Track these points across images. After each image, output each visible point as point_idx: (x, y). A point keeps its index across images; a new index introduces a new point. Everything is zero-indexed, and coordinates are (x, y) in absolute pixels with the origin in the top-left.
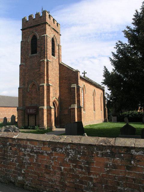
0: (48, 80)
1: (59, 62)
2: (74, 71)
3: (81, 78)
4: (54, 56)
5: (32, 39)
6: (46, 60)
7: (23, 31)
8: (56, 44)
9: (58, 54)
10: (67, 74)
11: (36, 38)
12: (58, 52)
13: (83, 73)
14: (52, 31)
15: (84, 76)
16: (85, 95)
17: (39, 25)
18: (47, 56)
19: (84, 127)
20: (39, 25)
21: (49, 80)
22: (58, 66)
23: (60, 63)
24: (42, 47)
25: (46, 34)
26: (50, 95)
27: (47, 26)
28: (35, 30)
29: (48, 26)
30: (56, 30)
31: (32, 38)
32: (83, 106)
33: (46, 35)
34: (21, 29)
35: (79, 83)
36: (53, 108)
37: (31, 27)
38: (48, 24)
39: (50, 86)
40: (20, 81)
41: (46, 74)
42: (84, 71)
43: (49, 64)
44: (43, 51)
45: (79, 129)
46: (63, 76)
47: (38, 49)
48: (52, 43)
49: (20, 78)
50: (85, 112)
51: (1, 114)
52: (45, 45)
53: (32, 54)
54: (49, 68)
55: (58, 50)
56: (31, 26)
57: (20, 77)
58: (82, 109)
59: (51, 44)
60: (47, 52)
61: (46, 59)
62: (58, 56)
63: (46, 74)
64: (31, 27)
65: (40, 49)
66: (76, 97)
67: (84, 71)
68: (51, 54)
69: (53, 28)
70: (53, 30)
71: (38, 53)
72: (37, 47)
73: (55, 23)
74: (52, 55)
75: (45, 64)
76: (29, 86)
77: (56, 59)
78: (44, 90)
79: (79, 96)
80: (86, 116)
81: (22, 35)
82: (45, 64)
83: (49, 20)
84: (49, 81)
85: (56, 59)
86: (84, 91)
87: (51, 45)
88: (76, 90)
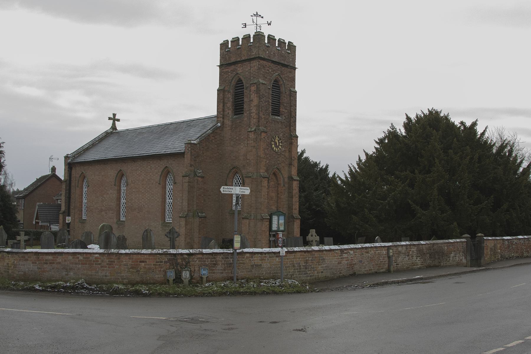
42: (110, 119)
44: (293, 118)
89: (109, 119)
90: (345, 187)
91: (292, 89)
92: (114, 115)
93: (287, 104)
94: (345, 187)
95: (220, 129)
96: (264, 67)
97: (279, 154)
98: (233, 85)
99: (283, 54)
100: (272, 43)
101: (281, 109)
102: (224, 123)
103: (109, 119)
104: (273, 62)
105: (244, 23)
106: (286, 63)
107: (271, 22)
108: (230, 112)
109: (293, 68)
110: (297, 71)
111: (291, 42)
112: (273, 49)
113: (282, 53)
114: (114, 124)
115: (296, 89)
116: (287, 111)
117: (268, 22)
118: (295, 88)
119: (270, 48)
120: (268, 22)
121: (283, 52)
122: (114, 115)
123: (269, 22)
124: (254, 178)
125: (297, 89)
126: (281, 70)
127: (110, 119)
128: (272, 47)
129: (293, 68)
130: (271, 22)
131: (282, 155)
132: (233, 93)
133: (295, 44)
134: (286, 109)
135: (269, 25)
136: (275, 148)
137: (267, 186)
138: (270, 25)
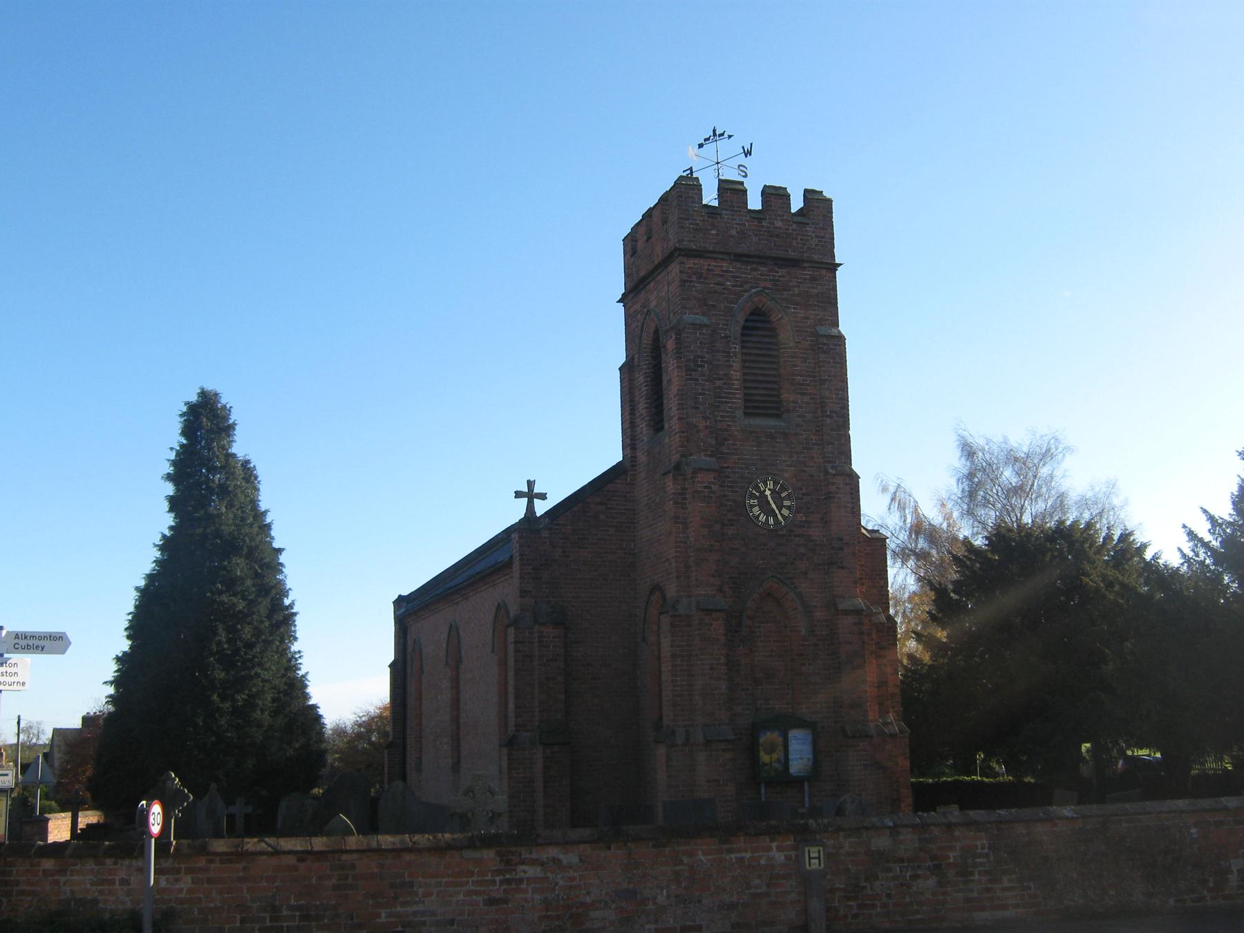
17: (795, 263)
42: (519, 494)
44: (830, 416)
89: (516, 497)
90: (1222, 601)
91: (822, 330)
92: (531, 484)
93: (809, 376)
94: (1222, 601)
95: (626, 480)
96: (700, 276)
97: (784, 535)
98: (645, 348)
99: (780, 228)
100: (730, 204)
101: (785, 396)
102: (636, 462)
103: (516, 497)
104: (739, 257)
105: (688, 167)
106: (791, 254)
107: (751, 144)
108: (643, 427)
109: (823, 266)
110: (839, 273)
111: (813, 191)
112: (735, 220)
113: (776, 228)
114: (530, 507)
115: (840, 328)
116: (806, 399)
117: (743, 147)
118: (838, 326)
119: (721, 218)
120: (743, 147)
121: (779, 224)
122: (531, 484)
123: (747, 147)
124: (680, 616)
125: (844, 328)
126: (775, 276)
127: (519, 494)
128: (733, 215)
129: (823, 266)
130: (751, 144)
131: (796, 536)
132: (649, 369)
133: (827, 194)
134: (802, 394)
135: (746, 156)
136: (762, 518)
137: (723, 637)
138: (750, 155)
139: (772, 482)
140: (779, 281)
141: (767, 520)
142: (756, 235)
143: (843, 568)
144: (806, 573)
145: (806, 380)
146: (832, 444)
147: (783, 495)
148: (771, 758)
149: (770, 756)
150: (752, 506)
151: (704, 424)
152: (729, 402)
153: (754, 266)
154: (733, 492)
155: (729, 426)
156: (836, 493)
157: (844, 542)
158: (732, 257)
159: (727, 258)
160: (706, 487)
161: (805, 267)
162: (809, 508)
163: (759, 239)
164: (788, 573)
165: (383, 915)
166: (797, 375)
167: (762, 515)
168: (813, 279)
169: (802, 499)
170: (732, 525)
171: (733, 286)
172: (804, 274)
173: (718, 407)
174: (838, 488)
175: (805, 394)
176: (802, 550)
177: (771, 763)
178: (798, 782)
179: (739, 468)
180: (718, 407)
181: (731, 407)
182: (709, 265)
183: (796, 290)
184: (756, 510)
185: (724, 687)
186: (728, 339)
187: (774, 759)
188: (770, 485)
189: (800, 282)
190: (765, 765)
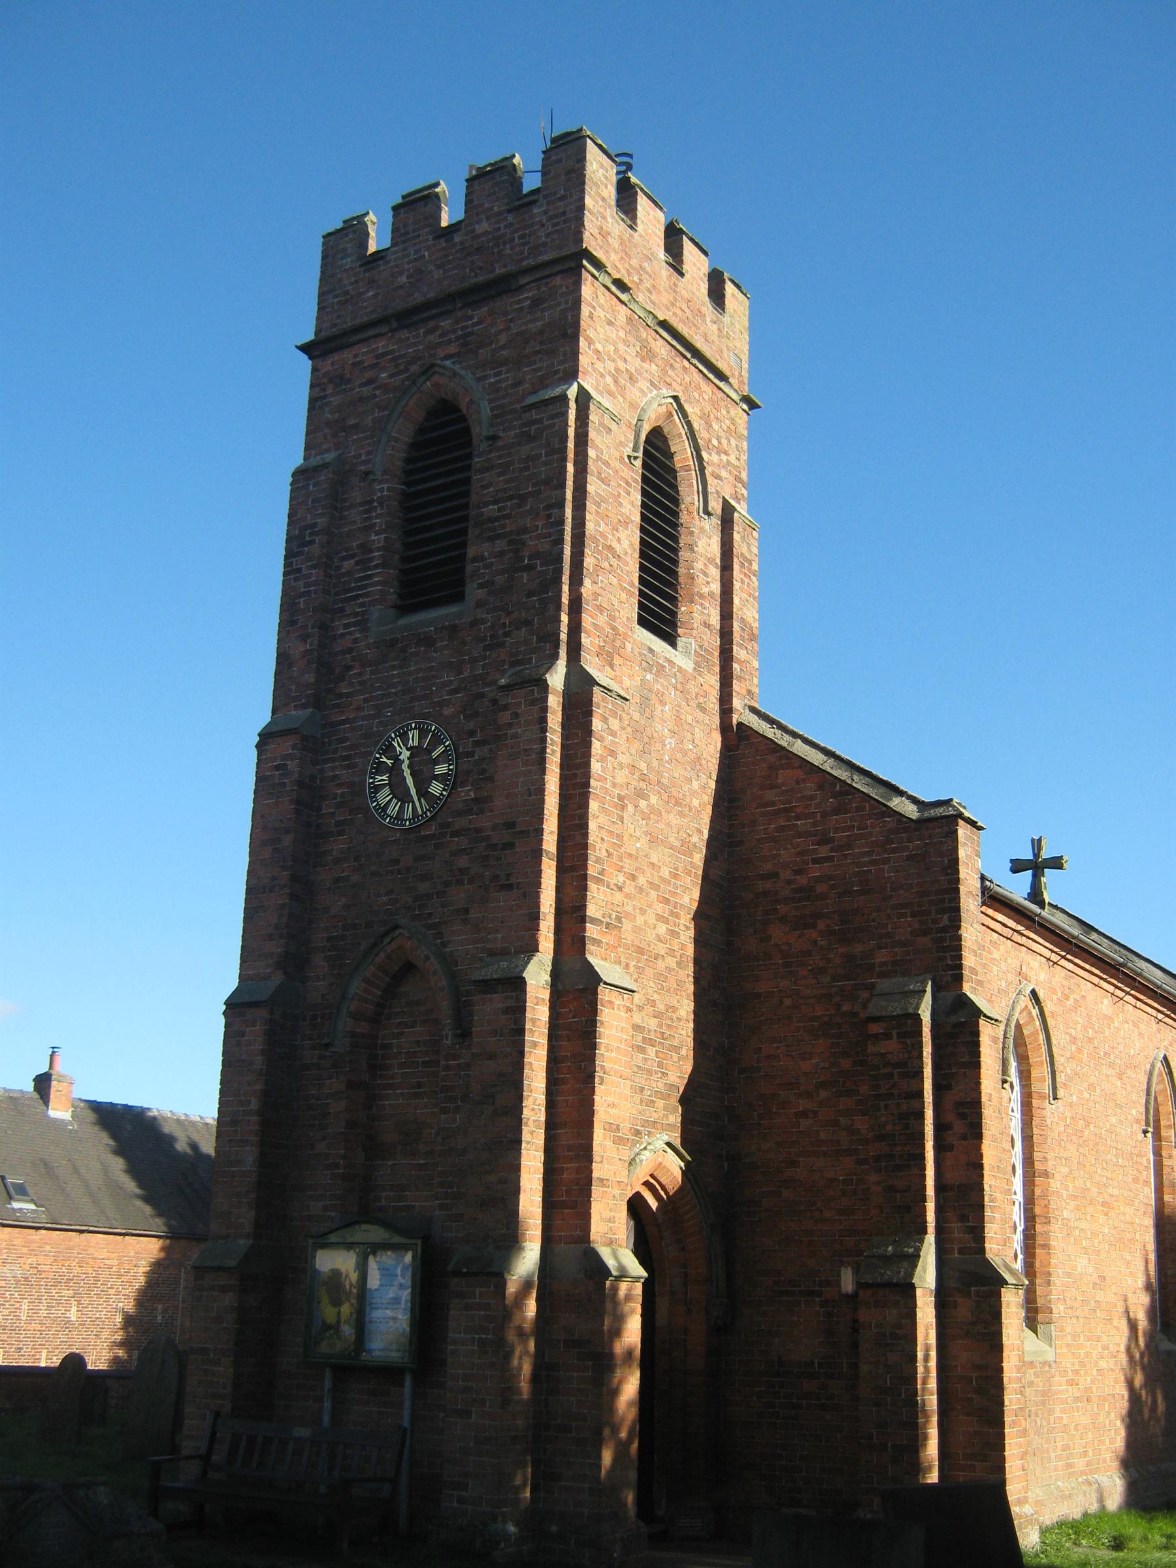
0: (583, 919)
1: (726, 708)
2: (910, 811)
3: (993, 899)
4: (670, 638)
5: (414, 446)
6: (556, 678)
7: (327, 365)
8: (689, 496)
9: (715, 619)
10: (824, 851)
11: (467, 431)
12: (716, 587)
13: (1017, 866)
14: (648, 355)
15: (1036, 895)
16: (1050, 1114)
17: (502, 286)
18: (575, 629)
19: (1029, 1539)
20: (502, 286)
21: (592, 910)
22: (711, 746)
23: (741, 714)
24: (528, 522)
25: (572, 374)
26: (598, 1105)
27: (591, 290)
28: (453, 349)
29: (604, 298)
30: (699, 343)
31: (421, 430)
32: (1018, 1265)
33: (572, 392)
34: (309, 336)
35: (969, 960)
36: (637, 1279)
37: (407, 318)
38: (598, 265)
39: (604, 994)
40: (246, 919)
41: (550, 842)
42: (1037, 844)
43: (597, 724)
44: (529, 568)
45: (1041, 904)
46: (775, 875)
47: (471, 552)
48: (645, 479)
49: (249, 891)
50: (1049, 1340)
51: (73, 1315)
52: (561, 504)
53: (404, 609)
54: (596, 766)
55: (715, 573)
56: (418, 298)
57: (250, 872)
58: (1012, 1303)
59: (637, 535)
60: (577, 580)
61: (561, 667)
62: (714, 642)
63: (550, 842)
64: (407, 318)
65: (501, 545)
66: (661, 471)
67: (1037, 844)
68: (629, 609)
69: (664, 324)
70: (661, 346)
71: (474, 592)
72: (464, 532)
73: (686, 267)
74: (642, 622)
75: (555, 720)
76: (356, 986)
77: (687, 664)
78: (521, 1031)
79: (975, 1132)
80: (1059, 1383)
81: (313, 402)
82: (555, 720)
83: (614, 222)
84: (591, 930)
85: (687, 664)
86: (1040, 1072)
87: (631, 505)
88: (927, 1050)
97: (433, 836)
139: (416, 732)
140: (472, 333)
141: (401, 809)
142: (438, 267)
143: (509, 887)
144: (467, 911)
145: (504, 508)
146: (528, 623)
147: (435, 754)
148: (339, 1313)
149: (336, 1310)
150: (377, 789)
151: (302, 649)
152: (358, 596)
153: (431, 324)
154: (348, 767)
155: (356, 641)
156: (511, 725)
157: (518, 829)
158: (395, 325)
159: (384, 329)
160: (277, 768)
161: (524, 285)
162: (484, 771)
163: (445, 271)
164: (430, 914)
165: (1058, 1410)
166: (487, 504)
167: (395, 801)
168: (536, 303)
169: (472, 754)
170: (341, 833)
171: (391, 376)
172: (519, 302)
173: (342, 610)
174: (516, 715)
175: (499, 536)
176: (463, 862)
177: (338, 1322)
178: (388, 1373)
179: (364, 718)
180: (342, 610)
181: (362, 605)
182: (356, 356)
183: (503, 338)
184: (384, 796)
185: (250, 1159)
186: (371, 477)
187: (343, 1318)
188: (414, 738)
189: (511, 320)
190: (326, 1327)
